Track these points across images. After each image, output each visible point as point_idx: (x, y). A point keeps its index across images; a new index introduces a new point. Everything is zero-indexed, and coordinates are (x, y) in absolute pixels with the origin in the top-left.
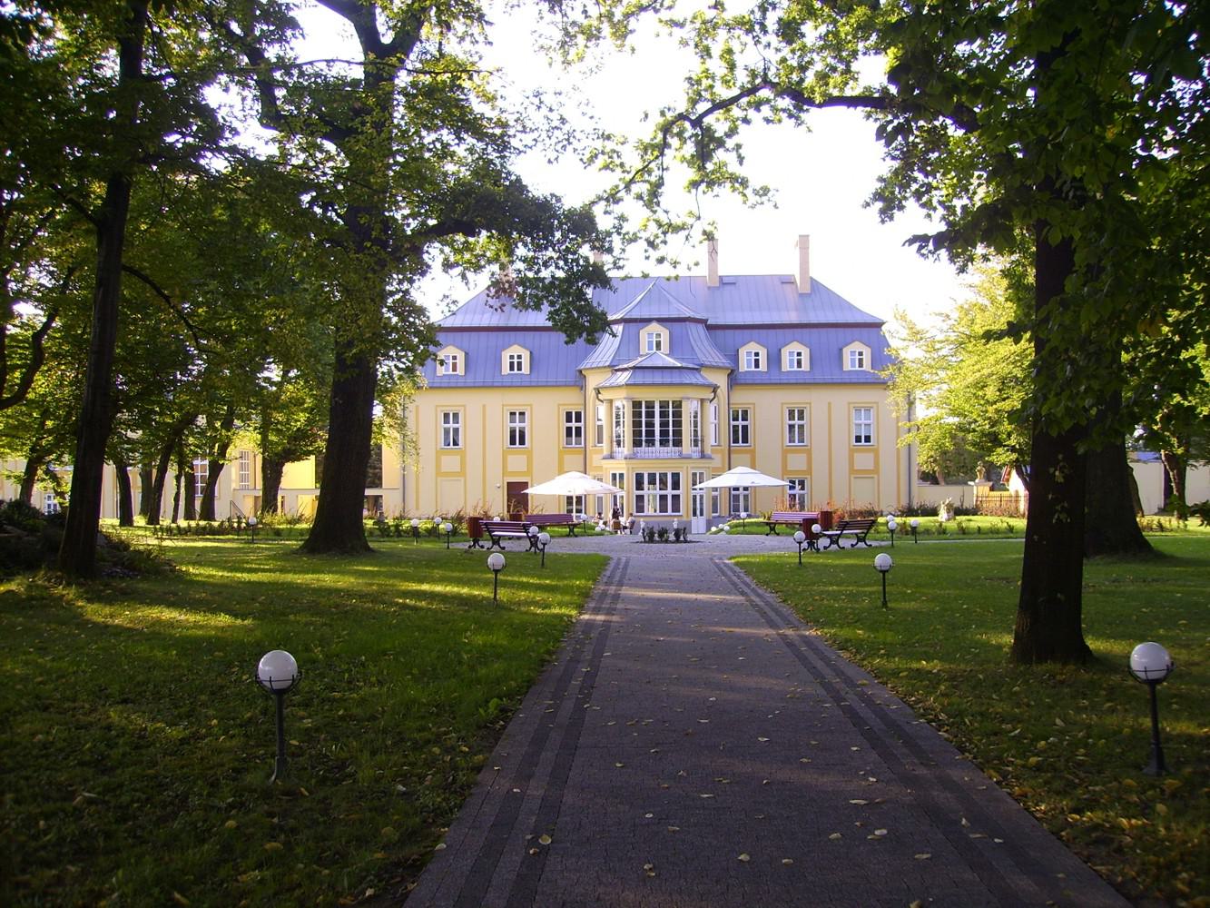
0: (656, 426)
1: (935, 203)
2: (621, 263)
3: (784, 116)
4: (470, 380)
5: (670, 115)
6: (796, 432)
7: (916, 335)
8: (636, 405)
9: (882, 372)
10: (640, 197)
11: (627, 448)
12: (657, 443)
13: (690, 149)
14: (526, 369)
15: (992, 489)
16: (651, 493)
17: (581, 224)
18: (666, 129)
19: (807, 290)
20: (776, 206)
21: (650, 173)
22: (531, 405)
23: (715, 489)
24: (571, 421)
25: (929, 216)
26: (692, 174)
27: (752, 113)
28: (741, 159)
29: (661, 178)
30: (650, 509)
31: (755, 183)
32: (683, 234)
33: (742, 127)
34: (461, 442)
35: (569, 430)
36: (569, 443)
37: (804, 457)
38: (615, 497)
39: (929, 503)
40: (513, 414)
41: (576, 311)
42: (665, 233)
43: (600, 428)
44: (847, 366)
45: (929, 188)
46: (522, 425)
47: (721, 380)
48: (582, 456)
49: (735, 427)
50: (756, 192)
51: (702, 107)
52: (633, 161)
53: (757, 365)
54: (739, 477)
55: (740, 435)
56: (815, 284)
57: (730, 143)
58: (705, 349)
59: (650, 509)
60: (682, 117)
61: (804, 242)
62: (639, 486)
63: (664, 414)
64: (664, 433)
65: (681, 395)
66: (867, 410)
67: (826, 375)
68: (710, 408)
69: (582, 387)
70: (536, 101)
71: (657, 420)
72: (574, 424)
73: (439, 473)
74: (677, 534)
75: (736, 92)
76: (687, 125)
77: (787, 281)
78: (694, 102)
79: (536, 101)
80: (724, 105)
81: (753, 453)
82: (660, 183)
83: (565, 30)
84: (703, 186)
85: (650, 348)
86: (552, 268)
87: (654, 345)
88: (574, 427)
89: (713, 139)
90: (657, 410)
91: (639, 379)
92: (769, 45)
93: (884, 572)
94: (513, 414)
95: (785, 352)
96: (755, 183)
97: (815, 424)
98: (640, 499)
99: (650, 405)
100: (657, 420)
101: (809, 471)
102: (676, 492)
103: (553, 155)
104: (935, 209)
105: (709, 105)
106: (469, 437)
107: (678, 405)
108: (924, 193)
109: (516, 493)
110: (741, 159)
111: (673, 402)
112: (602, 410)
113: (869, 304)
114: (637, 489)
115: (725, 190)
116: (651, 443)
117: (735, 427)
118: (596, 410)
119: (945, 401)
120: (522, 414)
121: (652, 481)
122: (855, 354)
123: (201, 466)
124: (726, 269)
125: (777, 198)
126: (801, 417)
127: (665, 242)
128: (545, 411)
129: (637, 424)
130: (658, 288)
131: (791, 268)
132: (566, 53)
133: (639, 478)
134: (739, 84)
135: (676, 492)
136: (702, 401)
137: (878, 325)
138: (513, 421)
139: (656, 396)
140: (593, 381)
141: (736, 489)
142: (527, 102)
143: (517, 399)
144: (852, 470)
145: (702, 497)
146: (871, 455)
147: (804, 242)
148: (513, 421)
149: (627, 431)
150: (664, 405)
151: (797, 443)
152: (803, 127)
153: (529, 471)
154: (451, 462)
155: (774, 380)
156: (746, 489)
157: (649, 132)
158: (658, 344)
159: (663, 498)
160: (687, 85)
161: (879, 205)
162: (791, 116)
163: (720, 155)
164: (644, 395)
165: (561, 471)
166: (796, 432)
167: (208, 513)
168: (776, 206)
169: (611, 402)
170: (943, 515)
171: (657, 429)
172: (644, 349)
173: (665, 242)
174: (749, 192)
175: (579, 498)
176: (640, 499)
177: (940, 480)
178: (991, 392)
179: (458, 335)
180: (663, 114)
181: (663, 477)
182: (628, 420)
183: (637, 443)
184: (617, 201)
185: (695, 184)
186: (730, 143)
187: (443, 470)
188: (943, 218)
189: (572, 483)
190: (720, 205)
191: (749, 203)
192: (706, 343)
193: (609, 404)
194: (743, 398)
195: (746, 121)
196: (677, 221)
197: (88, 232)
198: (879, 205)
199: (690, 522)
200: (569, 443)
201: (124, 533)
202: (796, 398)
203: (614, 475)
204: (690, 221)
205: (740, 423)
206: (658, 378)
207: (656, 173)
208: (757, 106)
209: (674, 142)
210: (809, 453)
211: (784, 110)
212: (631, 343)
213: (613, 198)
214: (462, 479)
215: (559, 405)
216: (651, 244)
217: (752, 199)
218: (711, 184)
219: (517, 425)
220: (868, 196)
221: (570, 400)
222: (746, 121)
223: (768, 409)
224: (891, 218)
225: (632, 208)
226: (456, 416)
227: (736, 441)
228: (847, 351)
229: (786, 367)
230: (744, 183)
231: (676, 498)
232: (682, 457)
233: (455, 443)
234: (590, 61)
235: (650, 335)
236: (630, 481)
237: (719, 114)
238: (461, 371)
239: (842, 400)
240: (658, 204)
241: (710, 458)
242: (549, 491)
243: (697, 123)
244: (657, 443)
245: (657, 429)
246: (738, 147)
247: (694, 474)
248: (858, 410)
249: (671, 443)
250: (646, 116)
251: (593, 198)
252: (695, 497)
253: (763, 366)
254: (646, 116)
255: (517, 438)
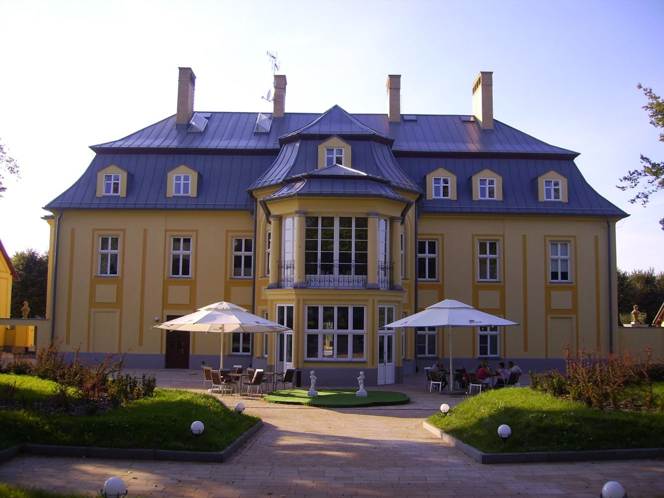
12: (336, 270)
16: (327, 332)
22: (197, 231)
24: (316, 327)
30: (327, 351)
34: (118, 270)
35: (238, 259)
36: (237, 273)
37: (496, 294)
38: (282, 336)
44: (543, 197)
46: (187, 252)
48: (251, 289)
59: (327, 351)
62: (313, 324)
65: (367, 210)
67: (521, 204)
73: (93, 303)
77: (465, 120)
88: (244, 262)
91: (316, 188)
98: (313, 339)
102: (358, 332)
106: (129, 266)
107: (362, 222)
111: (357, 219)
114: (310, 327)
120: (187, 241)
121: (328, 318)
124: (407, 108)
126: (493, 250)
133: (313, 313)
135: (358, 332)
138: (176, 248)
139: (336, 209)
143: (182, 224)
144: (549, 310)
145: (390, 338)
146: (569, 293)
148: (176, 248)
151: (488, 279)
155: (464, 208)
156: (432, 328)
159: (343, 339)
164: (321, 208)
176: (313, 339)
177: (259, 314)
181: (343, 311)
187: (97, 300)
192: (391, 165)
194: (431, 228)
199: (376, 370)
200: (237, 273)
202: (488, 229)
203: (281, 309)
210: (502, 289)
212: (308, 157)
214: (574, 316)
215: (227, 231)
221: (238, 225)
223: (458, 240)
229: (477, 196)
231: (358, 339)
232: (367, 287)
236: (301, 318)
238: (122, 192)
239: (537, 233)
241: (401, 290)
244: (336, 270)
247: (382, 311)
248: (554, 244)
249: (353, 269)
252: (382, 338)
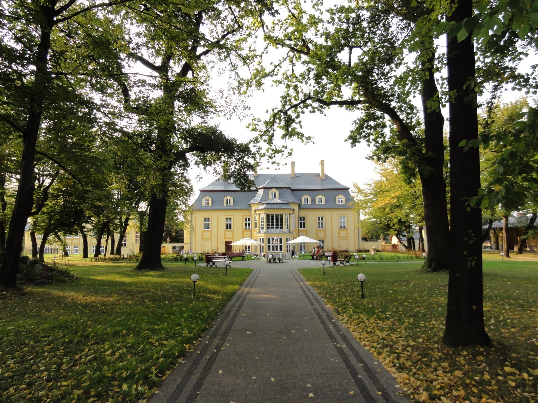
0: (274, 222)
1: (371, 140)
2: (259, 164)
3: (316, 110)
4: (213, 207)
5: (276, 111)
6: (321, 225)
7: (360, 191)
8: (268, 215)
9: (350, 205)
10: (265, 141)
11: (264, 230)
13: (283, 123)
14: (232, 204)
15: (386, 243)
17: (245, 149)
18: (274, 116)
19: (324, 178)
20: (314, 143)
21: (269, 132)
23: (294, 243)
25: (369, 145)
26: (283, 132)
27: (305, 110)
28: (301, 126)
29: (273, 134)
31: (306, 135)
32: (281, 154)
33: (301, 115)
35: (246, 224)
36: (246, 228)
37: (323, 232)
39: (366, 248)
40: (227, 219)
41: (244, 183)
42: (274, 153)
43: (256, 223)
44: (337, 203)
45: (369, 134)
47: (296, 207)
49: (301, 223)
50: (306, 138)
51: (287, 107)
52: (262, 127)
53: (308, 202)
54: (301, 239)
55: (302, 225)
56: (327, 177)
57: (297, 121)
58: (290, 198)
60: (280, 111)
61: (322, 163)
63: (277, 219)
64: (277, 225)
66: (344, 217)
67: (330, 206)
68: (292, 216)
69: (250, 210)
70: (221, 94)
71: (275, 220)
72: (247, 222)
73: (203, 238)
74: (279, 260)
75: (299, 101)
76: (282, 114)
77: (317, 175)
78: (284, 106)
79: (221, 94)
80: (296, 106)
81: (306, 231)
82: (273, 135)
83: (239, 82)
84: (287, 137)
85: (272, 197)
86: (234, 165)
87: (274, 197)
89: (291, 119)
90: (275, 217)
91: (269, 207)
92: (310, 85)
93: (362, 282)
94: (227, 219)
95: (317, 198)
96: (306, 135)
97: (327, 221)
99: (272, 215)
100: (275, 220)
101: (325, 237)
103: (228, 117)
104: (371, 142)
105: (289, 107)
107: (281, 215)
108: (367, 137)
109: (228, 246)
110: (301, 126)
112: (257, 217)
113: (344, 181)
115: (295, 138)
116: (273, 228)
117: (301, 223)
118: (255, 218)
119: (370, 213)
120: (230, 219)
122: (340, 199)
123: (117, 236)
124: (297, 171)
125: (314, 140)
126: (322, 219)
127: (275, 157)
128: (238, 219)
129: (268, 222)
130: (275, 178)
131: (318, 171)
132: (239, 90)
133: (269, 240)
134: (300, 99)
136: (290, 214)
137: (347, 189)
138: (227, 221)
139: (275, 213)
140: (254, 208)
141: (301, 243)
142: (217, 95)
143: (229, 214)
144: (339, 237)
146: (346, 232)
147: (322, 163)
148: (227, 221)
149: (265, 224)
150: (277, 215)
152: (323, 114)
153: (233, 238)
154: (207, 234)
155: (314, 208)
157: (267, 117)
158: (275, 195)
160: (281, 99)
161: (351, 141)
162: (319, 110)
163: (294, 125)
164: (270, 212)
165: (243, 237)
166: (321, 225)
167: (119, 251)
168: (314, 143)
169: (259, 214)
170: (372, 253)
171: (275, 223)
172: (270, 197)
173: (275, 157)
174: (304, 139)
175: (249, 247)
178: (387, 210)
179: (210, 193)
180: (273, 110)
182: (265, 221)
183: (268, 228)
184: (258, 142)
185: (285, 136)
186: (297, 121)
188: (374, 145)
189: (246, 241)
190: (294, 143)
191: (304, 143)
193: (259, 217)
194: (303, 213)
195: (303, 112)
196: (278, 149)
197: (20, 136)
198: (351, 141)
200: (246, 228)
201: (66, 260)
202: (321, 213)
203: (260, 239)
204: (283, 149)
205: (302, 221)
206: (275, 206)
207: (272, 132)
208: (307, 107)
209: (277, 121)
211: (316, 108)
213: (256, 141)
216: (270, 157)
217: (305, 141)
218: (290, 136)
219: (229, 222)
220: (346, 137)
221: (246, 214)
222: (303, 112)
224: (355, 146)
225: (264, 146)
226: (209, 219)
227: (301, 227)
228: (337, 198)
229: (317, 203)
230: (302, 136)
233: (208, 228)
234: (248, 94)
235: (272, 193)
236: (266, 241)
237: (293, 109)
239: (335, 214)
240: (272, 143)
242: (239, 244)
243: (285, 113)
245: (275, 223)
246: (300, 122)
248: (341, 217)
250: (267, 111)
251: (249, 141)
253: (310, 203)
254: (267, 111)
255: (229, 226)
